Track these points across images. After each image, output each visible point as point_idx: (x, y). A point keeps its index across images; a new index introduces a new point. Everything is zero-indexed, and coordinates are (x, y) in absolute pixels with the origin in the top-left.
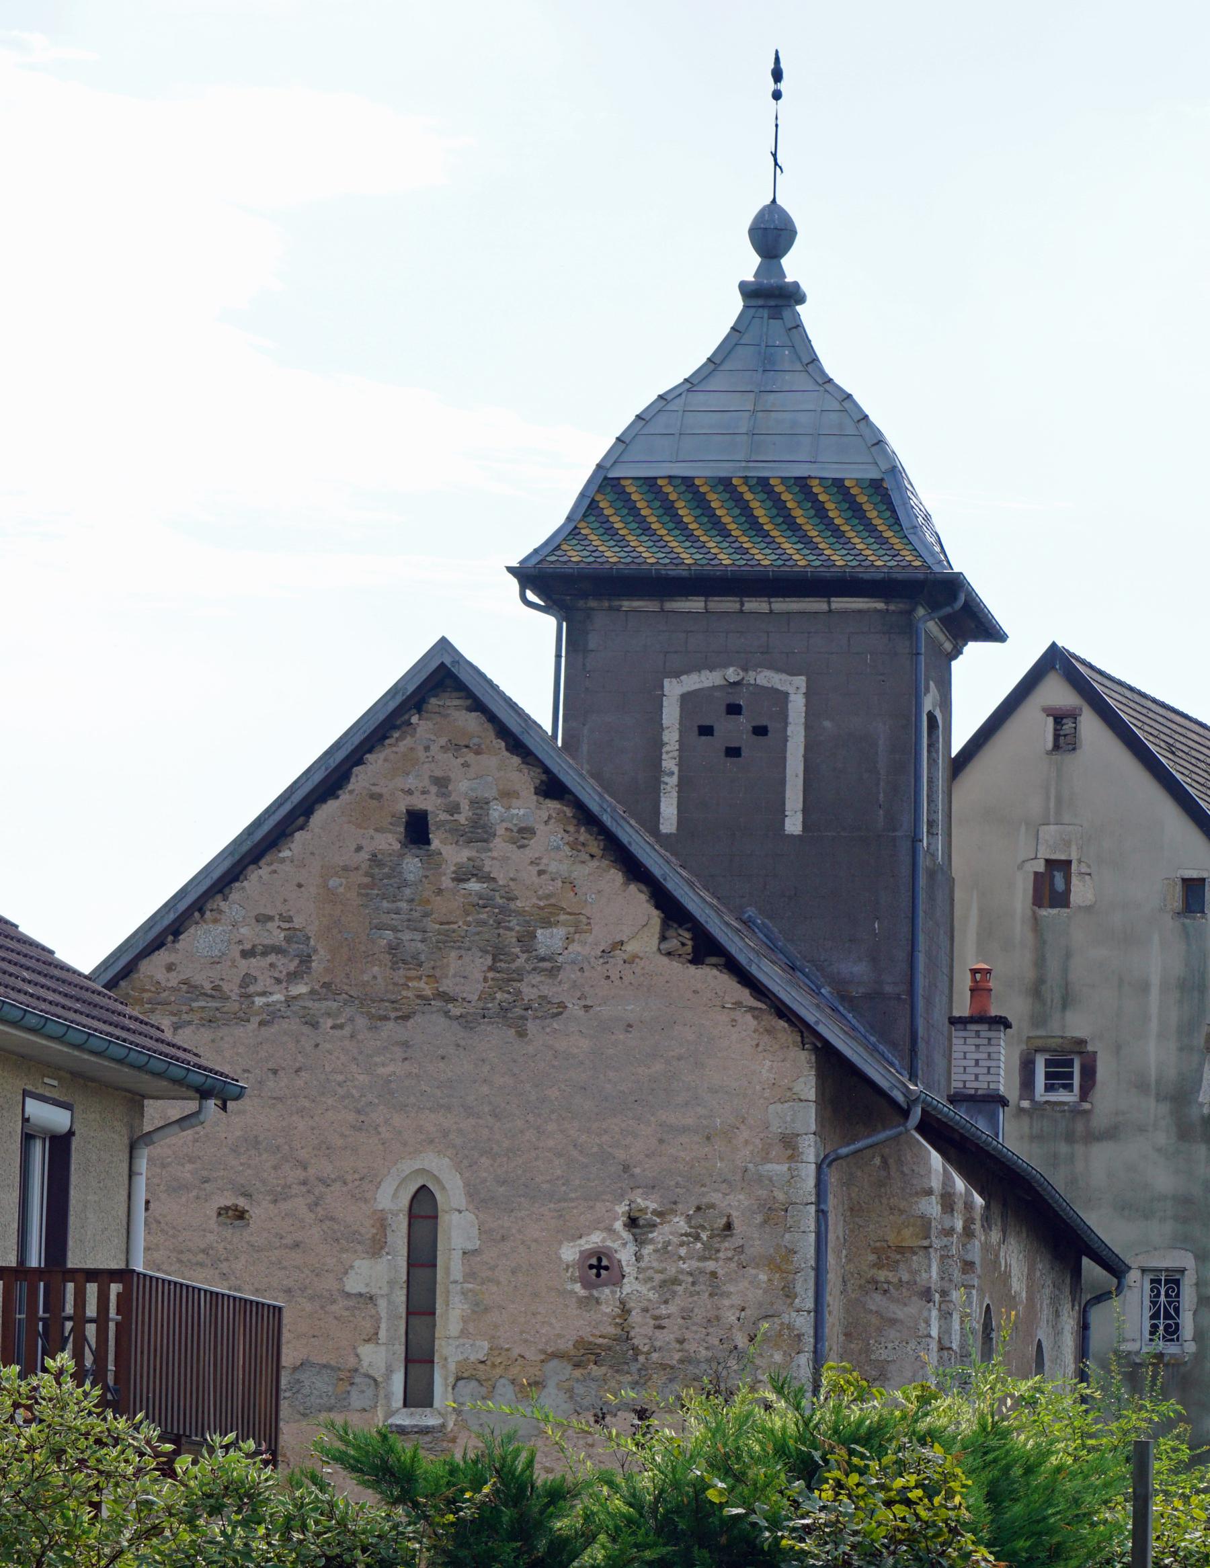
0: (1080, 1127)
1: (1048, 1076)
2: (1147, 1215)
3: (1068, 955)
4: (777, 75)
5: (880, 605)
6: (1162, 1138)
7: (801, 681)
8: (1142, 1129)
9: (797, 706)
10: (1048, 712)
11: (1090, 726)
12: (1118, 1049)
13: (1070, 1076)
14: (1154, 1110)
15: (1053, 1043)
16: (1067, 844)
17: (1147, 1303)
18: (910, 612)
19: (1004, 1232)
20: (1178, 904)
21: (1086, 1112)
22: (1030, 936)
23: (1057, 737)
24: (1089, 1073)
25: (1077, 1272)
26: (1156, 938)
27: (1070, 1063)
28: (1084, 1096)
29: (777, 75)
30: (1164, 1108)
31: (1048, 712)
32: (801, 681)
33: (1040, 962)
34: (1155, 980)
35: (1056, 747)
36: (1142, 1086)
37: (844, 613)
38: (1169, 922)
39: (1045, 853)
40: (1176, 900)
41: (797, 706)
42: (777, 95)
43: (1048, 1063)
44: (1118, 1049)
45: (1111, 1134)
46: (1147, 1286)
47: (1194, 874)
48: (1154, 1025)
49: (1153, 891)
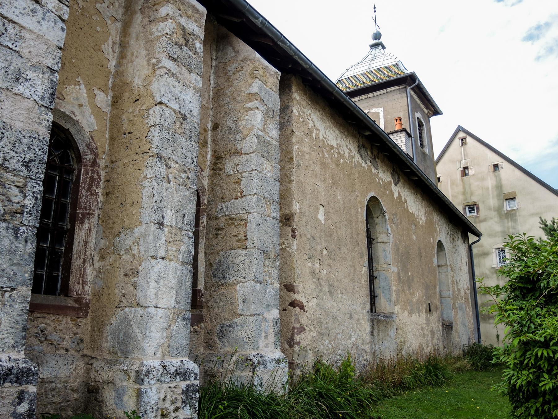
0: (477, 220)
1: (469, 211)
2: (495, 236)
3: (470, 185)
4: (375, 8)
5: (398, 88)
6: (496, 219)
7: (382, 109)
8: (491, 218)
9: (382, 115)
10: (459, 138)
11: (469, 139)
12: (484, 202)
13: (474, 210)
14: (493, 214)
15: (469, 204)
16: (467, 163)
17: (498, 256)
18: (405, 87)
19: (399, 178)
20: (493, 170)
21: (478, 217)
22: (461, 183)
23: (462, 143)
24: (478, 208)
25: (467, 237)
26: (489, 178)
27: (474, 208)
28: (477, 214)
29: (375, 8)
30: (496, 213)
31: (459, 138)
32: (382, 109)
33: (464, 188)
34: (490, 188)
35: (462, 145)
36: (490, 209)
37: (390, 92)
38: (492, 174)
39: (462, 166)
40: (492, 168)
41: (382, 115)
42: (375, 12)
43: (469, 208)
44: (484, 202)
45: (484, 220)
46: (497, 252)
47: (496, 163)
48: (491, 196)
49: (487, 167)
